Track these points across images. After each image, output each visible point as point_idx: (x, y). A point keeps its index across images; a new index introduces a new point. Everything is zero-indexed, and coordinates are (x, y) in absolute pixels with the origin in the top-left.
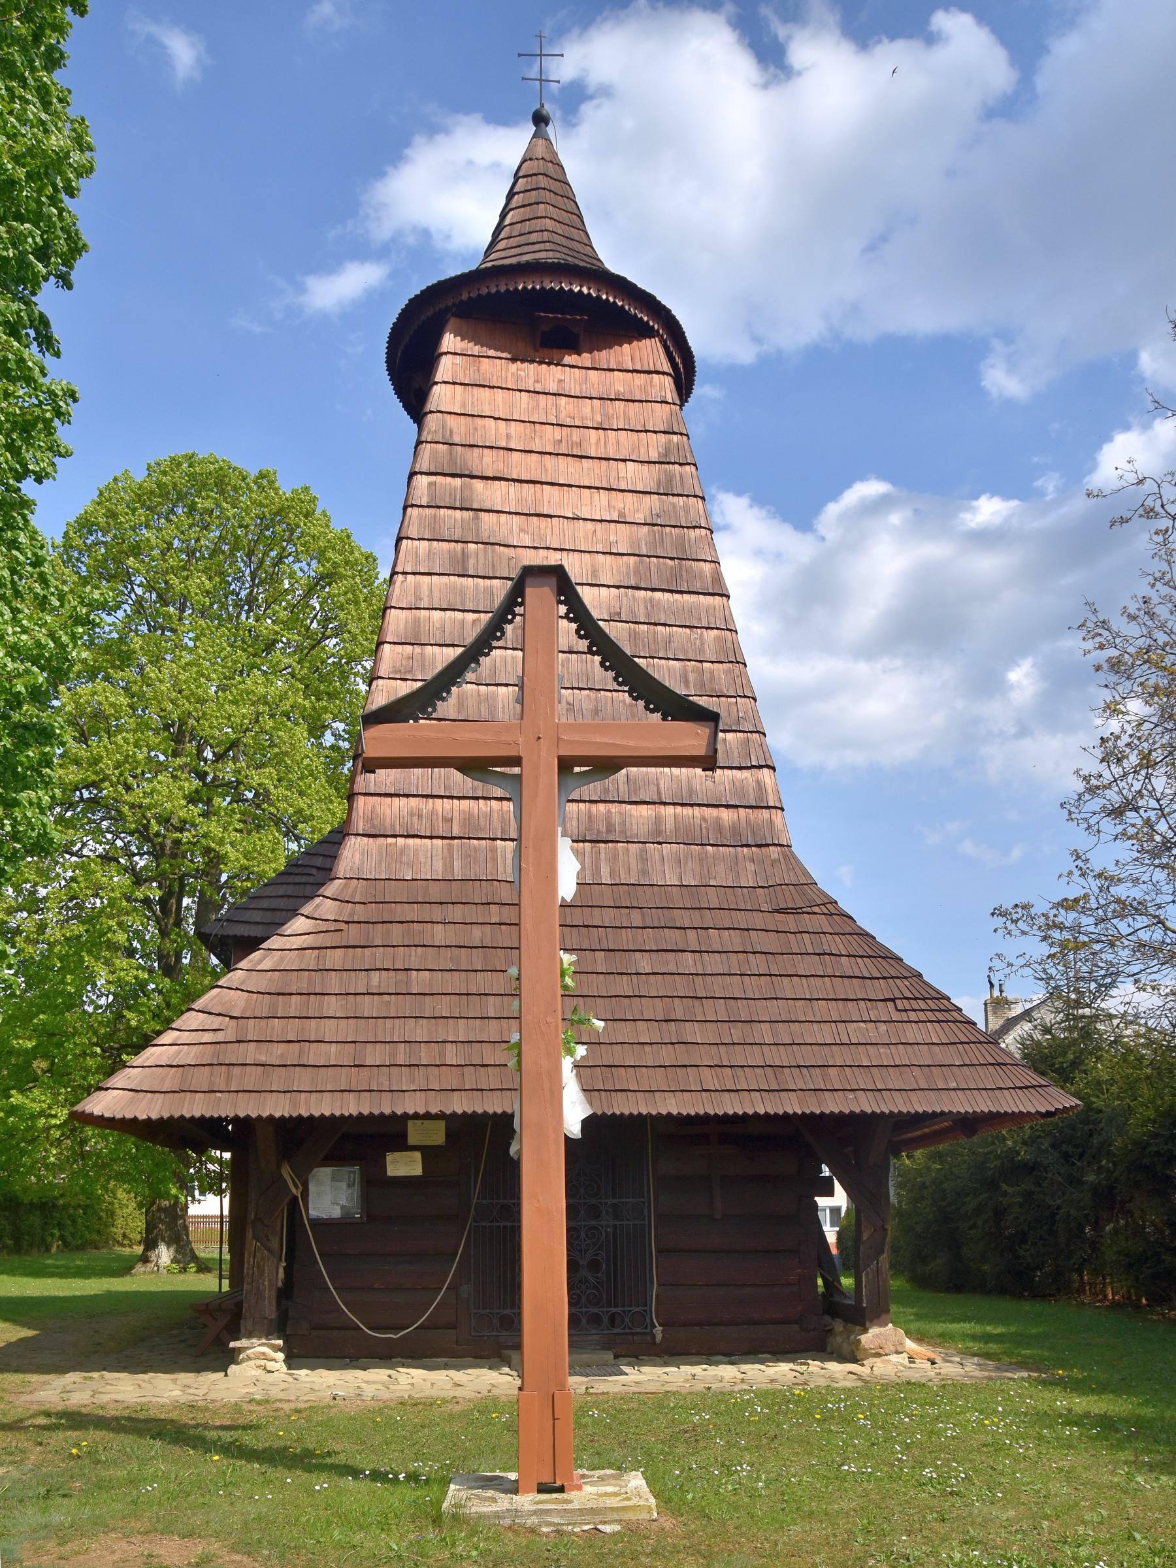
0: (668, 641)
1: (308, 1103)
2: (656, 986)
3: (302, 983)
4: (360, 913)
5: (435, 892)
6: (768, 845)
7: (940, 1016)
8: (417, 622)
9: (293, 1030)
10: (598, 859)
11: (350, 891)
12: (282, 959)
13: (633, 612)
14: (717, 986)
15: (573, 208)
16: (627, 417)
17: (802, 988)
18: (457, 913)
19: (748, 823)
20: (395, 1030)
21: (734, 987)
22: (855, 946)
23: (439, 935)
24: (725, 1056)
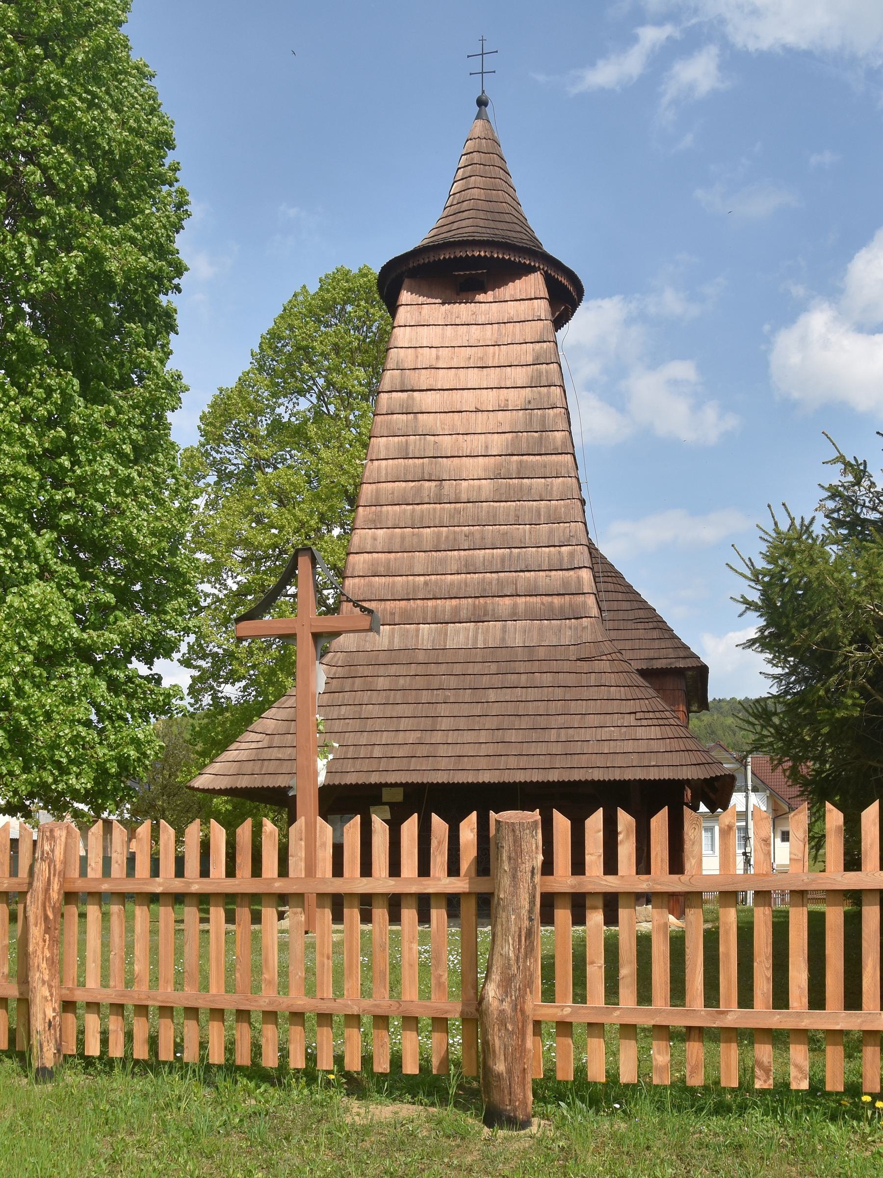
5: (383, 657)
6: (582, 618)
7: (661, 722)
8: (378, 491)
10: (477, 633)
11: (336, 659)
16: (514, 334)
19: (570, 605)
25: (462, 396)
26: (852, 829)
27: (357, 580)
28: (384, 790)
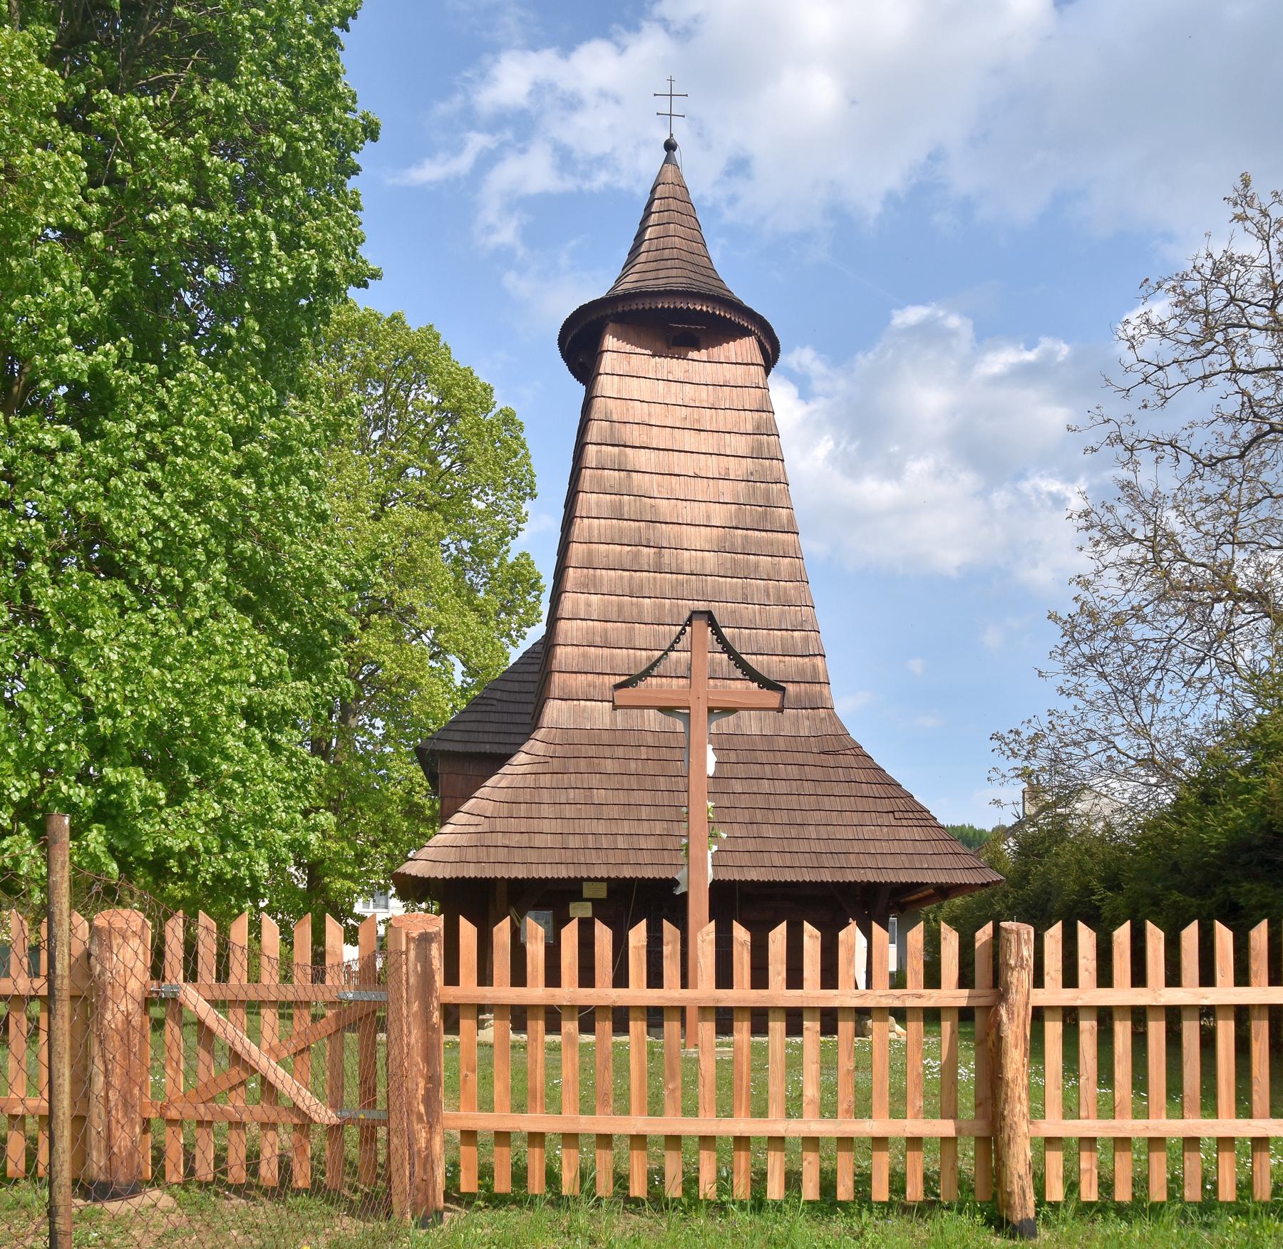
0: (757, 566)
1: (537, 871)
2: (745, 801)
3: (526, 796)
4: (559, 751)
5: (606, 738)
7: (922, 823)
8: (590, 553)
9: (523, 825)
12: (513, 780)
13: (732, 544)
14: (783, 802)
15: (693, 223)
16: (731, 399)
17: (837, 803)
18: (620, 752)
20: (586, 826)
21: (794, 802)
22: (871, 777)
23: (609, 766)
24: (786, 846)
25: (679, 458)
26: (1173, 947)
27: (569, 649)
28: (584, 884)
